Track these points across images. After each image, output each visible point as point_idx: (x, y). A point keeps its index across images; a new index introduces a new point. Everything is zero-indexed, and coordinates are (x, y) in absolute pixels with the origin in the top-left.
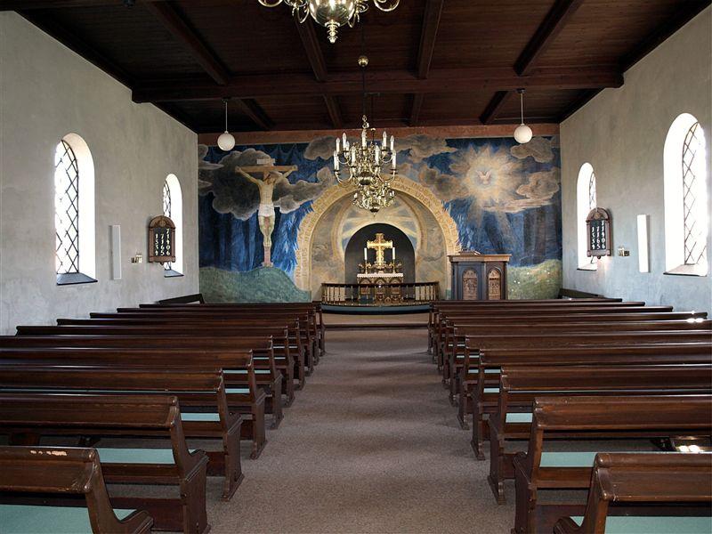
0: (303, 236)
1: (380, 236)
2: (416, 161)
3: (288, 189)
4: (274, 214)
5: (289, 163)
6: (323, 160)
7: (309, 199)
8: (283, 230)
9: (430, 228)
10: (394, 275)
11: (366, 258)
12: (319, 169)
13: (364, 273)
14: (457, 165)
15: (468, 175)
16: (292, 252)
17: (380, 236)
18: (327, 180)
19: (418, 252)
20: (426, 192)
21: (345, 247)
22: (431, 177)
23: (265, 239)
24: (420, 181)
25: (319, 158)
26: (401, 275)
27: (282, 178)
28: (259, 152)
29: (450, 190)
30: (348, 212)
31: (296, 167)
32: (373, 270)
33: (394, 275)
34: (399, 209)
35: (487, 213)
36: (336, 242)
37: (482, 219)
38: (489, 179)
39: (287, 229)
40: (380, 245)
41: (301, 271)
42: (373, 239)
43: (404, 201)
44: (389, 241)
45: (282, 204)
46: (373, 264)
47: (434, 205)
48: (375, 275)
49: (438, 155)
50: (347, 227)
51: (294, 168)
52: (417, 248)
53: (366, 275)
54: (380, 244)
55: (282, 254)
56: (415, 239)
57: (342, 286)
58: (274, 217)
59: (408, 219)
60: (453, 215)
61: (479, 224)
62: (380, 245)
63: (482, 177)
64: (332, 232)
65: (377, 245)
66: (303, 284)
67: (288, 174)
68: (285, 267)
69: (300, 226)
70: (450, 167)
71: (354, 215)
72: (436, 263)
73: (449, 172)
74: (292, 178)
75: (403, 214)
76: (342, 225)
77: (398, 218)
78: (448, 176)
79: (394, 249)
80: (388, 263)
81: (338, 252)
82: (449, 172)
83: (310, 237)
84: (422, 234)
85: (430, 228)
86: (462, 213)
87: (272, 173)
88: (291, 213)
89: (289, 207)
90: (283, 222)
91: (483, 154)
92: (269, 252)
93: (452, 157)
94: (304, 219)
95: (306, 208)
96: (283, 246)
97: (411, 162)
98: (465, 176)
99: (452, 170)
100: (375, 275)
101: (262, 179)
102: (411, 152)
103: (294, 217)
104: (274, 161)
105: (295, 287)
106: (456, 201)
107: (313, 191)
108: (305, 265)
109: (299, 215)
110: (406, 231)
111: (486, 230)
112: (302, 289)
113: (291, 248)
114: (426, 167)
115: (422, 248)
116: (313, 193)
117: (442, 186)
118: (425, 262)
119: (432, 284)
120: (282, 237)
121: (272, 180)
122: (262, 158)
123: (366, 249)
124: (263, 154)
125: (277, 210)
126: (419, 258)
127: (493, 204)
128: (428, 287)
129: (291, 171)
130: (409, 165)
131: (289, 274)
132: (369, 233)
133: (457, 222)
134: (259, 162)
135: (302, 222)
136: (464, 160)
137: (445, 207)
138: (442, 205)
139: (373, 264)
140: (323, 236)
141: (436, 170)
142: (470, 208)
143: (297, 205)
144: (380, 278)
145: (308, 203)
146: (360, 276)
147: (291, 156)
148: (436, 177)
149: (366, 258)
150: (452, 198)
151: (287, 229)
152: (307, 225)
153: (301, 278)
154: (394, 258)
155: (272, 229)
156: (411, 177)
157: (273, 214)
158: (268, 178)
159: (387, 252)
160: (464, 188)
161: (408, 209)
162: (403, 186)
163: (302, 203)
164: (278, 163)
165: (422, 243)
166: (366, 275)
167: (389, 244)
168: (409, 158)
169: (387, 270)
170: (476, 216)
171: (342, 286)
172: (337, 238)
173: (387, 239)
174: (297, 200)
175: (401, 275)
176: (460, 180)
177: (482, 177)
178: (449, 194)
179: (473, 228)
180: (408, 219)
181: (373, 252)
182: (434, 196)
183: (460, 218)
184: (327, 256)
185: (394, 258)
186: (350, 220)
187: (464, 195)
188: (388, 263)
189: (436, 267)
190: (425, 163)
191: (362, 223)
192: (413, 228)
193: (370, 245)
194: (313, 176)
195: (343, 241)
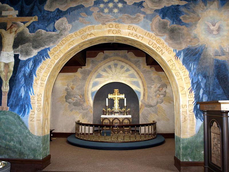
0: (39, 82)
1: (116, 90)
2: (149, 12)
3: (27, 38)
4: (13, 60)
5: (30, 14)
6: (61, 11)
7: (47, 47)
8: (20, 75)
9: (150, 86)
10: (125, 116)
11: (107, 105)
12: (57, 20)
13: (106, 115)
14: (187, 16)
15: (198, 25)
16: (27, 97)
17: (116, 90)
18: (65, 29)
19: (141, 102)
20: (158, 41)
21: (94, 97)
22: (163, 28)
23: (4, 84)
24: (153, 31)
25: (58, 9)
26: (130, 116)
27: (23, 27)
28: (5, 5)
29: (181, 40)
30: (96, 74)
31: (37, 17)
32: (112, 113)
33: (125, 116)
34: (129, 73)
35: (218, 61)
36: (88, 94)
37: (213, 68)
38: (219, 30)
39: (24, 75)
40: (117, 96)
41: (35, 116)
42: (112, 92)
43: (133, 68)
44: (122, 94)
45: (21, 52)
46: (112, 109)
47: (166, 53)
48: (113, 116)
49: (169, 8)
50: (95, 84)
51: (35, 19)
52: (141, 98)
53: (107, 116)
54: (116, 96)
55: (18, 98)
56: (140, 93)
57: (91, 125)
58: (13, 63)
59: (135, 80)
60: (185, 62)
61: (211, 71)
62: (117, 96)
63: (212, 28)
64: (85, 87)
65: (119, 96)
66: (36, 128)
67: (28, 24)
68: (20, 112)
69: (37, 72)
70: (181, 18)
71: (99, 76)
72: (153, 109)
73: (180, 22)
74: (32, 28)
75: (132, 76)
76: (92, 83)
77: (129, 79)
78: (180, 27)
79: (125, 99)
80: (121, 108)
81: (89, 100)
82: (180, 22)
83: (45, 83)
84: (144, 89)
85: (150, 86)
86: (195, 61)
87: (15, 23)
88: (29, 60)
89: (27, 53)
90: (21, 68)
91: (211, 6)
92: (7, 97)
93: (183, 9)
94: (41, 65)
95: (43, 55)
96: (20, 90)
97: (144, 13)
98: (196, 26)
99: (183, 21)
100: (113, 116)
101: (5, 28)
102: (144, 4)
103: (31, 63)
104: (17, 12)
105: (29, 132)
106: (188, 49)
107: (51, 39)
108: (39, 110)
109: (36, 61)
110: (134, 87)
111: (218, 78)
112: (36, 134)
113: (27, 93)
114: (158, 18)
115: (144, 98)
116: (51, 41)
117: (173, 35)
118: (146, 108)
119: (150, 124)
120: (19, 82)
121: (14, 29)
122: (7, 10)
123: (107, 99)
124: (8, 6)
125: (16, 57)
126: (142, 105)
127: (223, 53)
128: (147, 127)
129: (31, 21)
130: (142, 16)
131: (24, 119)
132: (110, 88)
133: (190, 70)
134: (4, 13)
135: (38, 69)
136: (194, 12)
137: (178, 55)
138: (175, 53)
139: (112, 109)
140: (79, 89)
141: (168, 21)
142: (202, 57)
143: (35, 53)
144: (116, 118)
145: (45, 50)
146: (103, 116)
147: (33, 8)
148: (168, 27)
149: (107, 105)
150: (184, 46)
151: (24, 75)
152: (43, 71)
153: (35, 123)
154: (125, 105)
155: (10, 75)
156: (144, 27)
157: (12, 60)
158: (11, 27)
159: (121, 101)
160: (195, 37)
161: (135, 73)
162: (136, 35)
163: (40, 50)
164: (21, 14)
165: (144, 95)
166: (107, 116)
167: (122, 96)
168: (142, 10)
169: (121, 113)
170: (208, 64)
171: (91, 125)
172: (88, 91)
173: (121, 93)
174: (35, 48)
175: (130, 116)
176: (191, 30)
177: (212, 28)
178: (181, 43)
179: (205, 76)
180: (135, 80)
181: (112, 101)
182: (166, 44)
183: (193, 66)
184: (81, 103)
185: (125, 105)
186: (97, 80)
187: (194, 45)
188: (121, 108)
189: (153, 112)
190: (158, 14)
191: (105, 81)
192: (138, 85)
193: (110, 96)
194: (51, 26)
195: (92, 93)
